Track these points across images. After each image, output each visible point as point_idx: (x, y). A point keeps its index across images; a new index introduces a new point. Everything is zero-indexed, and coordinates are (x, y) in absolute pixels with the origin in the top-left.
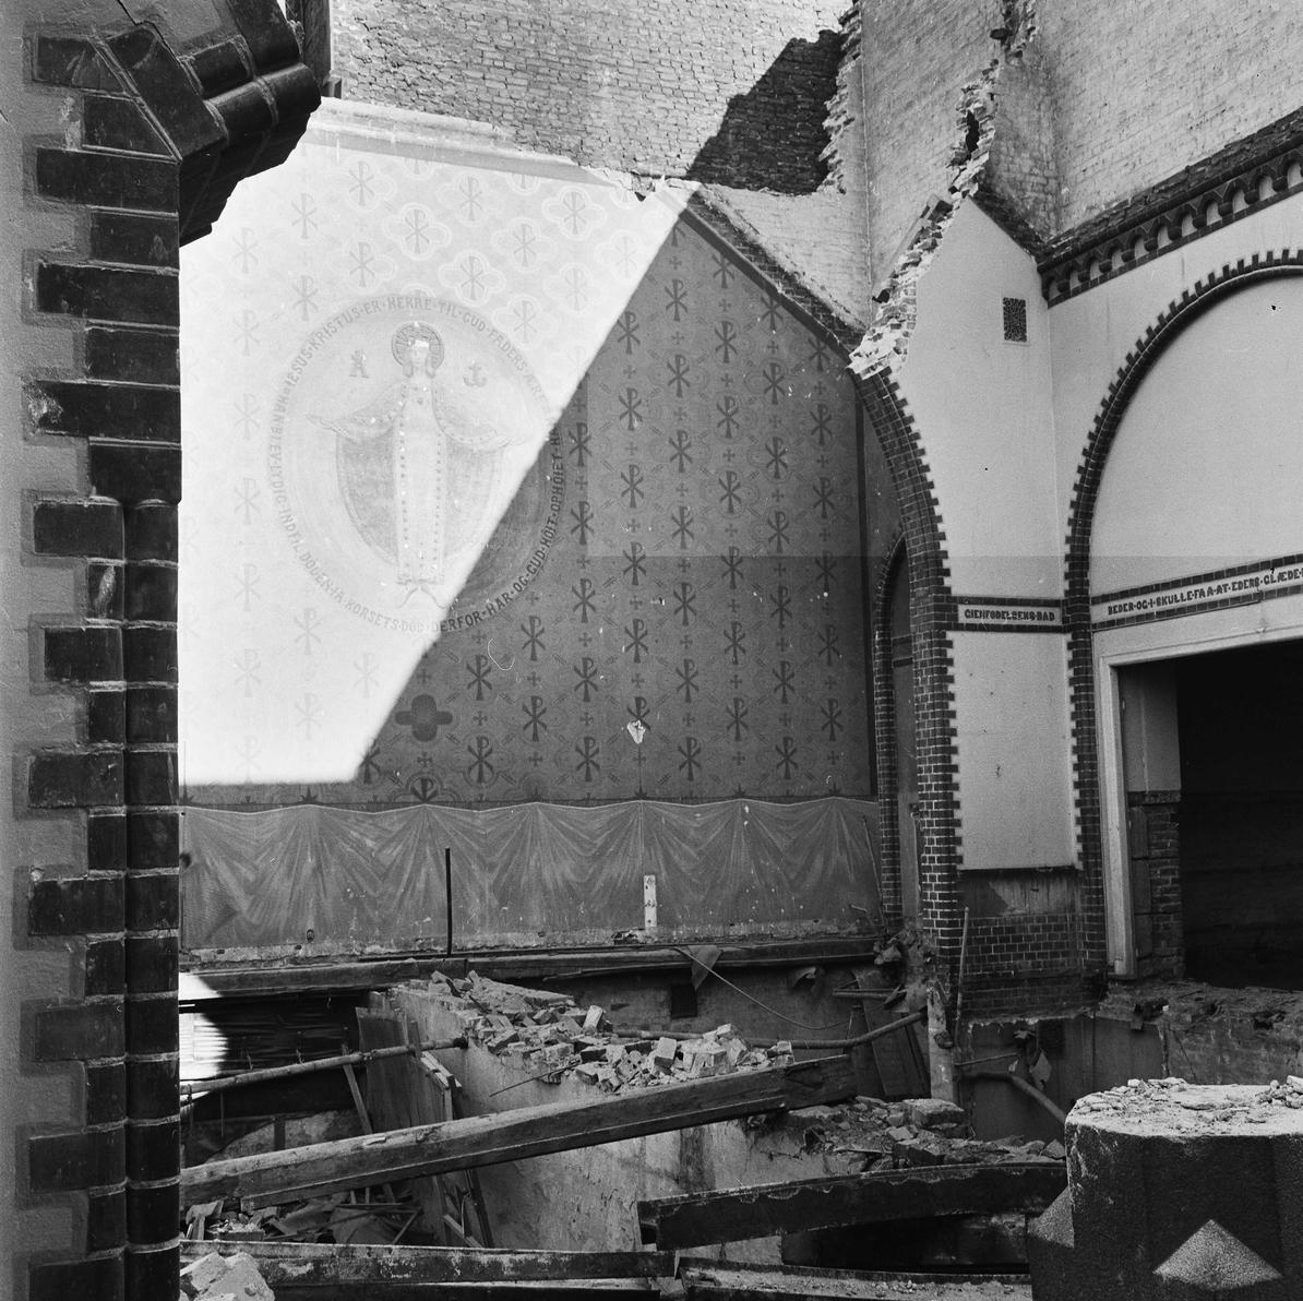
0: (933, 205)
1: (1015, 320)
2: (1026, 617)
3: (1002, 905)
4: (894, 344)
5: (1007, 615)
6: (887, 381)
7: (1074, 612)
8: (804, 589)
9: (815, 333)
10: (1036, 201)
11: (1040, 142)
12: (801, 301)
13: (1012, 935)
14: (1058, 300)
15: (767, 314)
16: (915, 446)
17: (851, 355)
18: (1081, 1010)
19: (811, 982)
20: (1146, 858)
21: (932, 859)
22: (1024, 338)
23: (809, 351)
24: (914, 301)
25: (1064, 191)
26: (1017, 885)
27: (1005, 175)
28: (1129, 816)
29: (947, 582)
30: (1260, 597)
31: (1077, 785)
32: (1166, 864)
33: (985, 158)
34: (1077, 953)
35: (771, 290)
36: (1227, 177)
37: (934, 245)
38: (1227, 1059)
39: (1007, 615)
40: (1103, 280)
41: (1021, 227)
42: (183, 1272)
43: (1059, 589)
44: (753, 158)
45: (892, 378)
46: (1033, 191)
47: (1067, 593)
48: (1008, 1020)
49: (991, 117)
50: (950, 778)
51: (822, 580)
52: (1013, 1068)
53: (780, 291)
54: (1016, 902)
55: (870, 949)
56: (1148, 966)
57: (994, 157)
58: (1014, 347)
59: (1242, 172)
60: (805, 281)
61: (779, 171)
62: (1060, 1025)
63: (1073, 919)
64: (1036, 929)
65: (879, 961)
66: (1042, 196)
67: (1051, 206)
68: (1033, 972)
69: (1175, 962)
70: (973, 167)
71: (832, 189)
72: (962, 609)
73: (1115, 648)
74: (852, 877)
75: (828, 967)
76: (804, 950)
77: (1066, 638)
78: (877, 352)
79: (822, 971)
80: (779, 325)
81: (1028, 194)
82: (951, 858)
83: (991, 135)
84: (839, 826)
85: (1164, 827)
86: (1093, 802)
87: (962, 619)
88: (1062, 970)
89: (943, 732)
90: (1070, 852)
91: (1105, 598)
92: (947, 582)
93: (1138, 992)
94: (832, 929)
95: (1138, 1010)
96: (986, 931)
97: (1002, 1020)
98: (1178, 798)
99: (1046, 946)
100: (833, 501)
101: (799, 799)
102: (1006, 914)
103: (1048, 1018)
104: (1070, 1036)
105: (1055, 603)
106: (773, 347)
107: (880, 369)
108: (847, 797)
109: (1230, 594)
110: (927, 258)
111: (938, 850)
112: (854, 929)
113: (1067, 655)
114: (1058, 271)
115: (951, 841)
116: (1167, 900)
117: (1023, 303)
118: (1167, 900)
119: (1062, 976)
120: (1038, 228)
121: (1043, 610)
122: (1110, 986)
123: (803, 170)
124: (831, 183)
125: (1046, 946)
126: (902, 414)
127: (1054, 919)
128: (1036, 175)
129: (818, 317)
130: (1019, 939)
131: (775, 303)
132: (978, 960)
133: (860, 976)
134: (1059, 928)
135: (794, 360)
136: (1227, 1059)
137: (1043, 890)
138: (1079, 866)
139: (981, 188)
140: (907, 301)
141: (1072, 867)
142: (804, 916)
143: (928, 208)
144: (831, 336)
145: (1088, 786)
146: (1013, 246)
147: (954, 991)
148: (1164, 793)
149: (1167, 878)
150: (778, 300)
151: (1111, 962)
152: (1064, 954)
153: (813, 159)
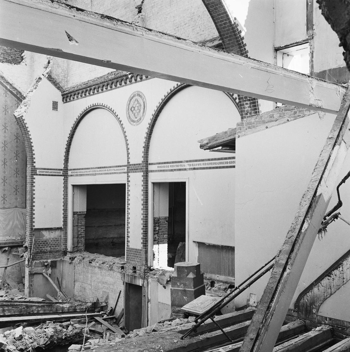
0: (38, 78)
1: (55, 106)
2: (54, 173)
3: (44, 236)
4: (25, 110)
5: (49, 172)
6: (22, 119)
7: (65, 173)
8: (11, 159)
9: (17, 98)
10: (62, 79)
11: (64, 66)
12: (14, 90)
13: (46, 243)
14: (65, 103)
15: (5, 93)
16: (28, 134)
17: (15, 111)
18: (61, 258)
19: (7, 251)
20: (77, 226)
21: (28, 226)
22: (57, 110)
23: (15, 102)
24: (30, 101)
25: (68, 78)
26: (47, 231)
27: (55, 73)
28: (73, 217)
29: (34, 164)
30: (96, 174)
31: (63, 210)
32: (82, 227)
33: (50, 69)
34: (61, 246)
35: (6, 88)
36: (93, 86)
37: (36, 88)
38: (84, 269)
39: (49, 172)
40: (73, 100)
41: (58, 85)
42: (18, 280)
43: (62, 167)
44: (5, 54)
45: (23, 118)
46: (61, 77)
47: (64, 168)
48: (43, 261)
49: (52, 59)
50: (33, 208)
51: (16, 157)
52: (44, 271)
53: (8, 88)
54: (47, 235)
55: (23, 243)
56: (76, 249)
57: (52, 69)
58: (54, 112)
59: (96, 85)
60: (15, 86)
61: (11, 57)
62: (56, 262)
63: (61, 238)
64: (52, 241)
65: (24, 246)
66: (64, 78)
67: (66, 81)
68: (50, 250)
69: (83, 248)
70: (48, 70)
71: (24, 64)
72: (38, 171)
73: (73, 181)
74: (19, 227)
75: (12, 247)
76: (5, 244)
77: (63, 177)
78: (20, 111)
79: (10, 248)
80: (7, 96)
81: (60, 78)
82: (32, 226)
83: (52, 63)
84: (17, 214)
85: (82, 219)
86: (66, 214)
87: (38, 173)
88: (57, 250)
89: (32, 198)
90: (61, 225)
91: (71, 170)
92: (34, 164)
93: (72, 254)
94: (14, 238)
95: (70, 259)
96: (40, 242)
97: (42, 261)
98: (85, 213)
99: (54, 244)
100: (19, 139)
101: (7, 208)
102: (45, 238)
103: (53, 260)
104: (58, 264)
105: (61, 170)
106: (6, 101)
107: (21, 116)
108: (19, 208)
109: (91, 173)
110: (34, 91)
111: (29, 224)
112: (19, 238)
113: (63, 181)
114: (65, 96)
115: (32, 222)
116: (82, 235)
117: (57, 102)
118: (82, 235)
119: (57, 251)
120: (62, 85)
121: (58, 171)
122: (67, 253)
123: (18, 57)
124: (24, 62)
125: (54, 244)
126: (25, 126)
127: (57, 239)
128: (62, 73)
129: (18, 94)
130: (48, 243)
131: (7, 91)
132: (37, 248)
133: (20, 249)
134: (58, 241)
135: (11, 105)
136: (84, 269)
137: (54, 232)
138: (63, 227)
139: (49, 76)
140: (28, 100)
141: (61, 228)
142: (6, 235)
143: (37, 78)
144: (21, 99)
145: (65, 210)
146: (56, 90)
147: (30, 255)
148: (82, 212)
149: (82, 230)
150: (7, 90)
151: (67, 248)
152: (58, 246)
153: (20, 55)
